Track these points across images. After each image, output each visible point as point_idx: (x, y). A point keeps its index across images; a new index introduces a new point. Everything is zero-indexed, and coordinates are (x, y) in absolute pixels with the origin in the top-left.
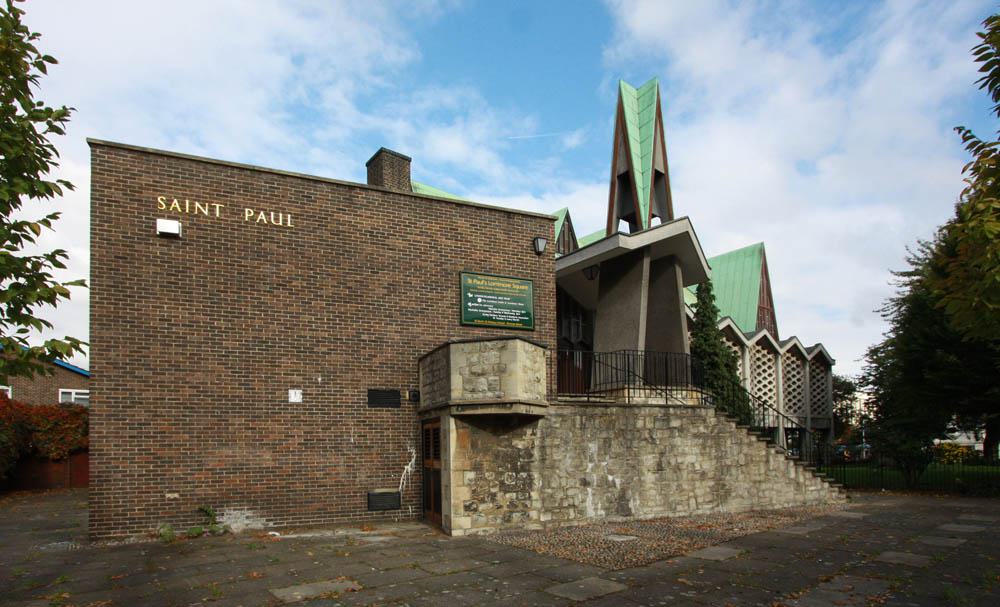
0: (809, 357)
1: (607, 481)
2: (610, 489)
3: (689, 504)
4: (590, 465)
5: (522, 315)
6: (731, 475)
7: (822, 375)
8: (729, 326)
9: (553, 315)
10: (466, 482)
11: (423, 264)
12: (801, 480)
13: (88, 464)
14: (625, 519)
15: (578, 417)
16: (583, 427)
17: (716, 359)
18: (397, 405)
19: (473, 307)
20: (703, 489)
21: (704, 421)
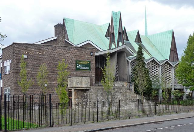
9: (94, 62)
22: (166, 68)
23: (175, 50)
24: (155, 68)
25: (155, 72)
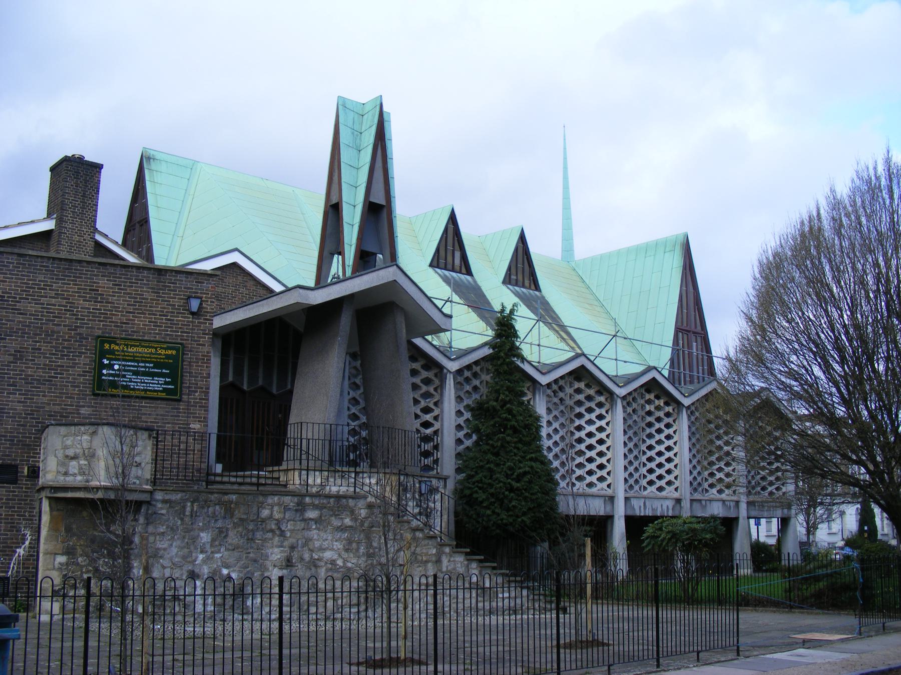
4: (201, 557)
5: (166, 383)
8: (583, 367)
10: (56, 566)
11: (56, 328)
13: (649, 516)
18: (14, 481)
22: (649, 413)
24: (590, 410)
25: (592, 428)
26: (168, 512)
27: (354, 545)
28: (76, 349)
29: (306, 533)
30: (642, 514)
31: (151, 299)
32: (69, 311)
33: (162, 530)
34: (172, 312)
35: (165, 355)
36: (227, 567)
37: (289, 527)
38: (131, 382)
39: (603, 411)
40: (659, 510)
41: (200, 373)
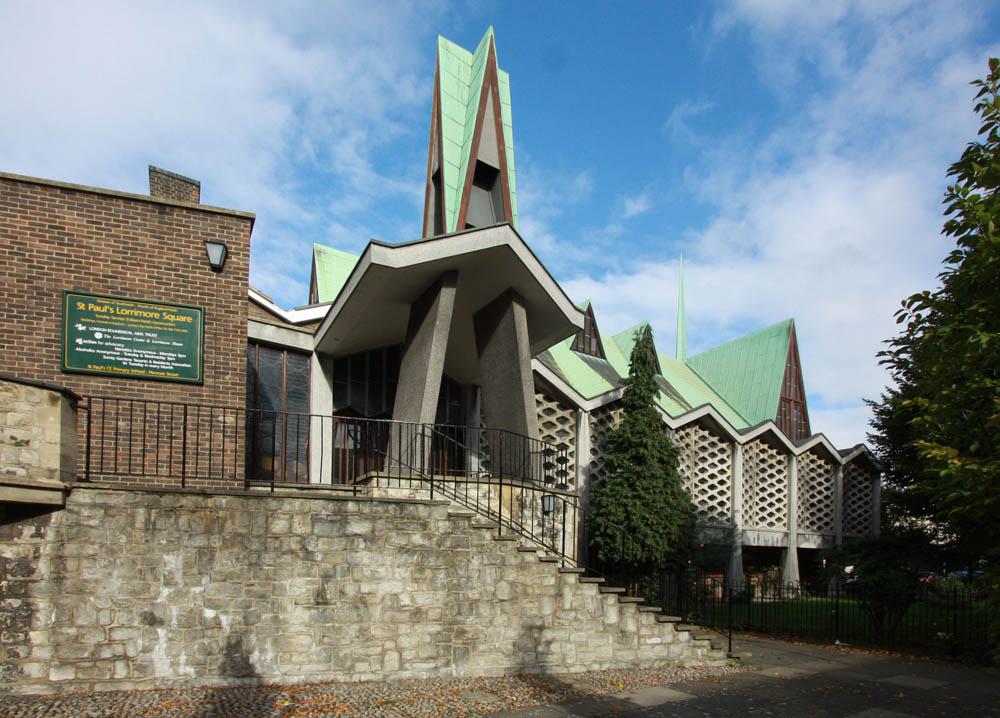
0: (843, 461)
1: (202, 620)
2: (209, 633)
3: (382, 662)
5: (178, 360)
6: (479, 615)
7: (867, 483)
8: (709, 415)
12: (631, 626)
14: (238, 682)
15: (141, 511)
16: (150, 528)
17: (641, 450)
19: (85, 346)
20: (414, 638)
21: (425, 526)
23: (799, 399)
26: (102, 522)
27: (428, 573)
28: (34, 308)
29: (348, 556)
30: (756, 544)
31: (150, 246)
32: (16, 254)
33: (91, 552)
34: (185, 266)
35: (174, 322)
36: (215, 607)
37: (321, 547)
38: (123, 356)
39: (724, 456)
40: (770, 541)
41: (232, 350)
